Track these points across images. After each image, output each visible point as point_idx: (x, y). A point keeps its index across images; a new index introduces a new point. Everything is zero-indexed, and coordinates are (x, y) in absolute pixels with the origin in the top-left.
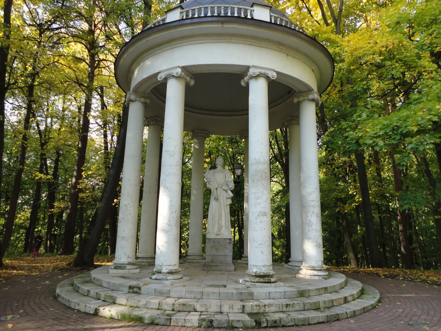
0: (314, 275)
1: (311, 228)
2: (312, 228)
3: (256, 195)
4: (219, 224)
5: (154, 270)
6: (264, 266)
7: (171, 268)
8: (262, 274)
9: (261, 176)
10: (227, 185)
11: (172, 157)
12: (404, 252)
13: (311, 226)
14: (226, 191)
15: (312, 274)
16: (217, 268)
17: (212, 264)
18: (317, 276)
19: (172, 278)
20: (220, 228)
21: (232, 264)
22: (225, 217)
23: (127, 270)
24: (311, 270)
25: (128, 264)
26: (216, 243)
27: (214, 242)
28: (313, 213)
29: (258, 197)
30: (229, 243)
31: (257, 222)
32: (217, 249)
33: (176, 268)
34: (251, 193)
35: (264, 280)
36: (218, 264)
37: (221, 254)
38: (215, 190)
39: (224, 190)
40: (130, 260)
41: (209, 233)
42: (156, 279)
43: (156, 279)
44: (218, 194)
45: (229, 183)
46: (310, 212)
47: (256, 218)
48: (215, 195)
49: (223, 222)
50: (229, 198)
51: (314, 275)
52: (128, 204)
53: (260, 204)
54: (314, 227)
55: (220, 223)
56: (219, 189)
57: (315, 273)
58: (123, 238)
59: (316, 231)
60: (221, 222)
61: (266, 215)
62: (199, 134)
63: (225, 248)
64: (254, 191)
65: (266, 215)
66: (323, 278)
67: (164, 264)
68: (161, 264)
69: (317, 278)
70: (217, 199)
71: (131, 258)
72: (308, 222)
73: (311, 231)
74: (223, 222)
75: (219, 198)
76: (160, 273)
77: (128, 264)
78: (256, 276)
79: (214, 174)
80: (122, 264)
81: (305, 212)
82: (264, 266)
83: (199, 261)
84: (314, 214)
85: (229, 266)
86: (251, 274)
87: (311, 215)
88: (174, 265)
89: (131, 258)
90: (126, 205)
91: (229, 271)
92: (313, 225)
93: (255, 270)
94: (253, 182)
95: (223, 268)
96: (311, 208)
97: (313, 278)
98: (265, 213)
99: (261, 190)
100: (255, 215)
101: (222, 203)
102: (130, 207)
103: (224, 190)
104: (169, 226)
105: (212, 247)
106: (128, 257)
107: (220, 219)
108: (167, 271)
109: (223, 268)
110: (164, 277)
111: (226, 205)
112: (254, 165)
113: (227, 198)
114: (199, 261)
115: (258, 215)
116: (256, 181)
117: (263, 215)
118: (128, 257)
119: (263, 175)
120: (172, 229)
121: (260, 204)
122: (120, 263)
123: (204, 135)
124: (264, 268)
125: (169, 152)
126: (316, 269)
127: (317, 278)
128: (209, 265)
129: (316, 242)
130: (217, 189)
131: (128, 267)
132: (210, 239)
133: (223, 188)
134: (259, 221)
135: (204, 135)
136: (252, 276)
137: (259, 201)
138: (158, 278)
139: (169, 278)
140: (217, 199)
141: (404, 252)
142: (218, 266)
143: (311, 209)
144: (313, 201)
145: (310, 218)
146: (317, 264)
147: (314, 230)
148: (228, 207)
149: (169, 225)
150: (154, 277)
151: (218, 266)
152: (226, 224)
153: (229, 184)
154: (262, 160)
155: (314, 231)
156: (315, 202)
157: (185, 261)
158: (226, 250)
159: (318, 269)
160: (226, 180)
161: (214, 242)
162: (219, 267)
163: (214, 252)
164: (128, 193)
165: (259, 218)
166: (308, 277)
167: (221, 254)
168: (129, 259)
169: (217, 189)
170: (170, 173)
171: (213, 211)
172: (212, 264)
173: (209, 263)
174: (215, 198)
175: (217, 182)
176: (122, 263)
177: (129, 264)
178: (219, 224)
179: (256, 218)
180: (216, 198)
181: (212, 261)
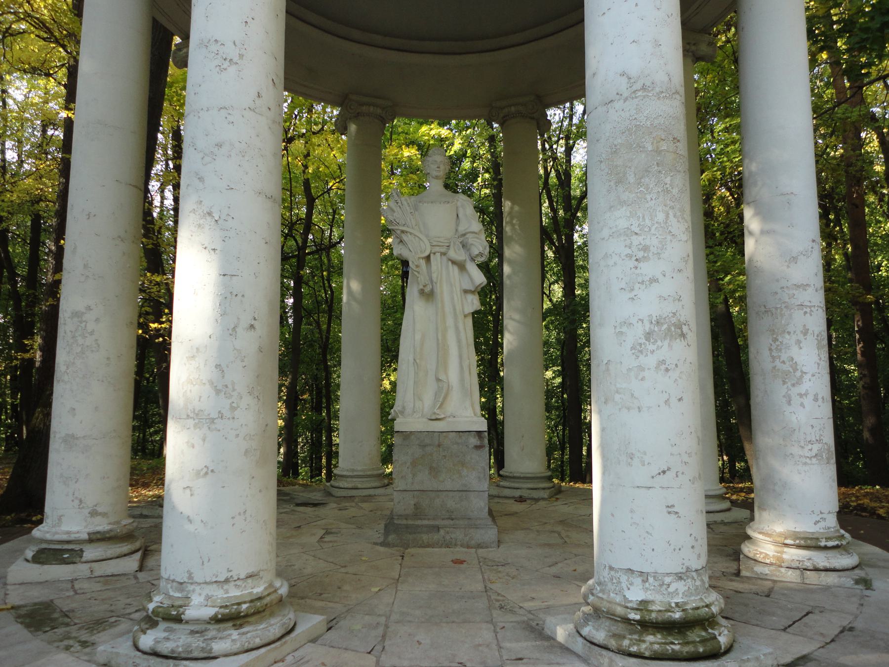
0: (816, 569)
1: (795, 391)
2: (802, 389)
3: (636, 240)
4: (438, 380)
5: (151, 606)
6: (680, 577)
7: (234, 593)
8: (677, 615)
9: (658, 151)
10: (464, 246)
11: (232, 69)
12: (871, 441)
13: (799, 381)
14: (461, 266)
15: (808, 564)
16: (436, 537)
17: (419, 522)
18: (827, 570)
19: (237, 647)
20: (442, 394)
21: (489, 521)
22: (461, 357)
23: (87, 566)
24: (799, 547)
25: (91, 541)
26: (428, 449)
27: (423, 446)
28: (805, 332)
29: (646, 249)
30: (478, 447)
31: (641, 368)
32: (434, 471)
33: (259, 589)
34: (606, 233)
35: (687, 649)
36: (437, 523)
37: (448, 485)
38: (423, 263)
39: (454, 262)
40: (101, 525)
41: (402, 412)
42: (156, 654)
43: (156, 654)
44: (434, 276)
45: (471, 239)
46: (791, 328)
47: (638, 350)
48: (423, 279)
49: (453, 375)
50: (472, 292)
51: (816, 569)
52: (89, 308)
53: (654, 280)
54: (807, 385)
55: (442, 377)
56: (436, 260)
57: (821, 559)
58: (70, 440)
59: (816, 399)
60: (446, 373)
61: (683, 335)
62: (364, 109)
63: (463, 464)
64: (623, 224)
65: (683, 335)
66: (857, 582)
67: (198, 577)
68: (182, 577)
69: (831, 579)
70: (428, 295)
71: (104, 515)
72: (786, 367)
73: (796, 400)
74: (453, 375)
75: (437, 290)
76: (178, 620)
77: (91, 541)
78: (646, 626)
79: (416, 208)
80: (68, 542)
81: (772, 331)
82: (680, 577)
83: (372, 492)
84: (809, 337)
85: (477, 527)
86: (620, 610)
87: (798, 342)
88: (250, 576)
89: (104, 515)
90: (77, 314)
91: (479, 546)
92: (807, 377)
93: (635, 595)
94: (619, 182)
95: (459, 535)
96: (798, 315)
97: (812, 578)
98: (679, 326)
99: (661, 217)
100: (637, 333)
101: (448, 308)
102: (97, 320)
103: (454, 262)
104: (218, 392)
105: (414, 464)
106: (94, 513)
107: (442, 362)
108: (210, 612)
109: (459, 535)
110: (196, 643)
111: (460, 317)
112: (618, 105)
113: (466, 292)
114: (372, 492)
115: (648, 335)
116: (631, 179)
117: (668, 334)
118: (94, 513)
119: (664, 146)
120: (233, 409)
121: (654, 280)
122: (57, 537)
123: (379, 111)
124: (680, 586)
125: (214, 48)
126: (823, 544)
127: (831, 579)
128: (407, 527)
129: (819, 441)
130: (428, 258)
131: (90, 553)
132: (406, 435)
133: (452, 254)
134: (650, 361)
135: (379, 111)
136: (626, 621)
137: (648, 269)
138: (165, 648)
139: (218, 647)
140: (428, 295)
141: (871, 441)
142: (437, 528)
143: (798, 319)
144: (804, 287)
145: (794, 352)
146: (822, 524)
147: (811, 397)
148: (469, 322)
149: (220, 389)
150: (147, 640)
151: (437, 528)
152: (462, 380)
153: (470, 241)
154: (660, 77)
155: (808, 401)
156: (810, 290)
157: (329, 494)
158: (465, 472)
159: (830, 544)
160: (462, 229)
161: (423, 446)
162: (442, 532)
163: (424, 480)
164: (86, 266)
165: (651, 347)
166: (791, 576)
167: (449, 487)
168: (98, 519)
169: (428, 258)
170: (219, 145)
171: (418, 337)
172: (419, 522)
173: (406, 517)
174: (422, 292)
175: (427, 236)
176: (65, 537)
177: (96, 538)
178: (438, 380)
179: (638, 350)
180: (427, 290)
181: (418, 512)
